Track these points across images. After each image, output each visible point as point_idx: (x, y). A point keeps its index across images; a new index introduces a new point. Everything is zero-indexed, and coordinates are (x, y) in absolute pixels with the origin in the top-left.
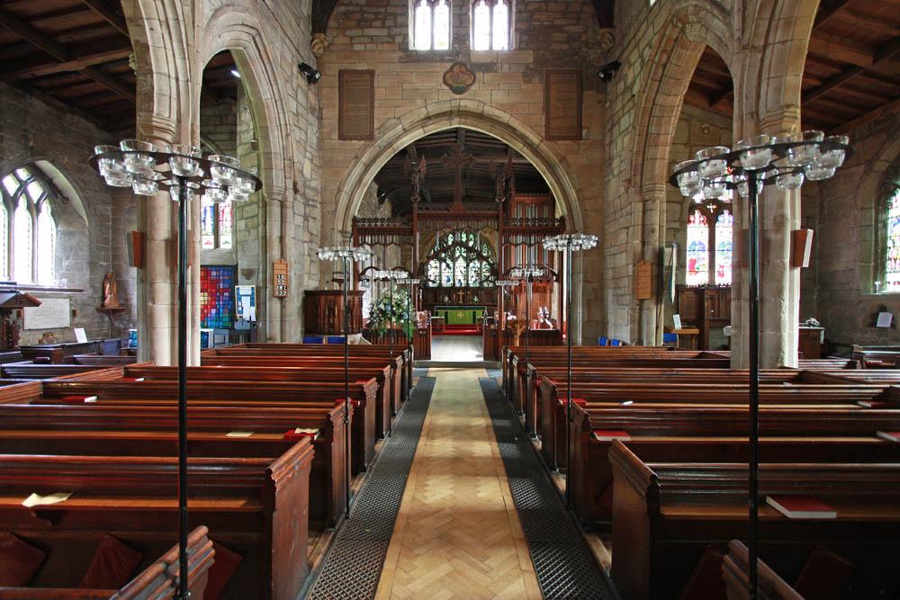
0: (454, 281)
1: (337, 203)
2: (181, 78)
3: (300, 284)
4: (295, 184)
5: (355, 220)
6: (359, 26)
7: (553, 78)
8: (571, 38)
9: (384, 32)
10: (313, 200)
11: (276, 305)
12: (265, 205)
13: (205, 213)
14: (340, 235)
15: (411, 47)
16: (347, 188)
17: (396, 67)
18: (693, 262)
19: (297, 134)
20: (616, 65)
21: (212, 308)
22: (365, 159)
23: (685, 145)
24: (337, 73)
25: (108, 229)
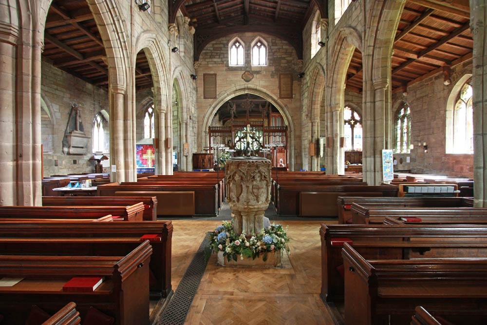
1: (203, 121)
2: (168, 95)
3: (192, 151)
4: (190, 117)
5: (209, 127)
6: (210, 58)
7: (282, 76)
8: (288, 62)
9: (219, 60)
11: (185, 158)
12: (180, 124)
14: (204, 133)
15: (230, 66)
16: (207, 116)
17: (225, 72)
19: (191, 99)
20: (303, 74)
22: (213, 106)
25: (57, 123)
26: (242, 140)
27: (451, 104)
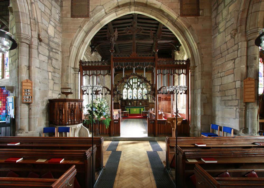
0: (132, 97)
1: (70, 52)
5: (81, 62)
10: (56, 49)
13: (7, 60)
21: (3, 110)
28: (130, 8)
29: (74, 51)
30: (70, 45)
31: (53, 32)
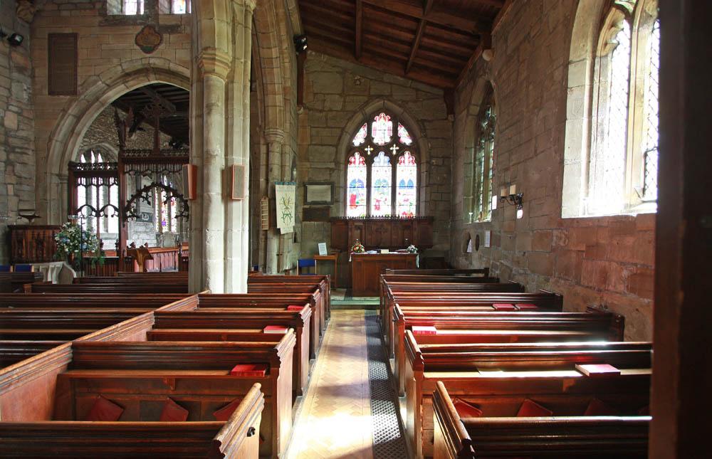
18: (354, 198)
23: (340, 95)
24: (47, 37)
26: (144, 194)
27: (584, 36)
28: (147, 76)
29: (56, 147)
30: (48, 139)
31: (16, 122)
